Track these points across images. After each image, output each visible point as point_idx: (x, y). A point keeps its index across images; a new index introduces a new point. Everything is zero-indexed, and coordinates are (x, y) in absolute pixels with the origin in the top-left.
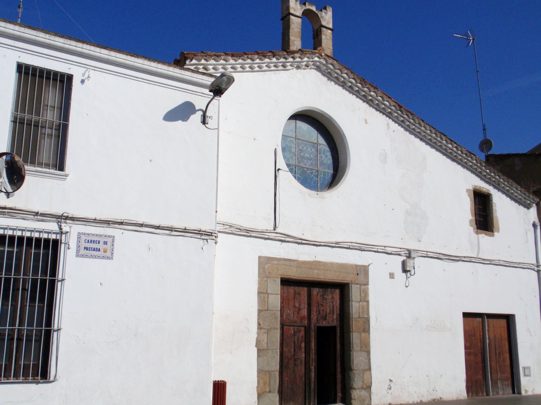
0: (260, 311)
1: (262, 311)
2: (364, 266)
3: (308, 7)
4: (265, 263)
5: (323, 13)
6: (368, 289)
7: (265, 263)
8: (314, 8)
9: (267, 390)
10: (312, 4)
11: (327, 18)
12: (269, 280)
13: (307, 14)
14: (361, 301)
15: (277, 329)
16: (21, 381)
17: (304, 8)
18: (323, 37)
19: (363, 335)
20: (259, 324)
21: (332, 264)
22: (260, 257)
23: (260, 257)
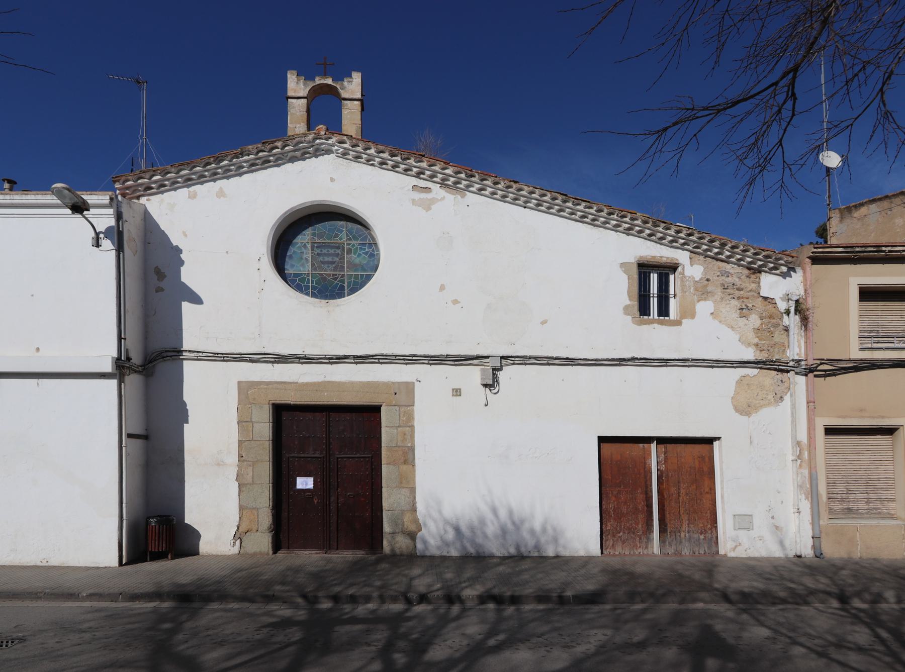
0: (240, 443)
1: (245, 441)
2: (407, 383)
3: (318, 81)
4: (245, 388)
5: (345, 83)
6: (413, 411)
7: (245, 388)
8: (329, 81)
9: (255, 528)
10: (325, 75)
11: (353, 86)
12: (254, 406)
13: (316, 94)
14: (399, 426)
15: (390, 449)
16: (577, 217)
17: (311, 85)
18: (345, 112)
19: (405, 468)
20: (241, 456)
21: (352, 383)
22: (239, 383)
23: (239, 383)
